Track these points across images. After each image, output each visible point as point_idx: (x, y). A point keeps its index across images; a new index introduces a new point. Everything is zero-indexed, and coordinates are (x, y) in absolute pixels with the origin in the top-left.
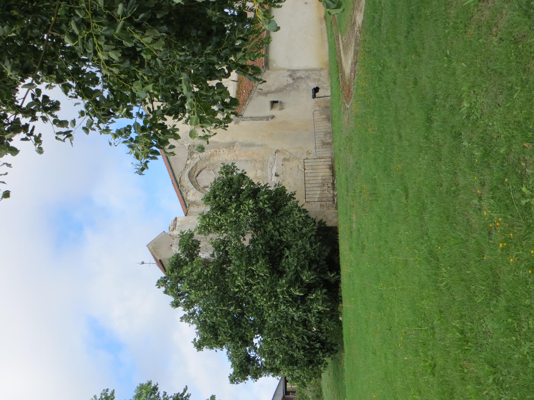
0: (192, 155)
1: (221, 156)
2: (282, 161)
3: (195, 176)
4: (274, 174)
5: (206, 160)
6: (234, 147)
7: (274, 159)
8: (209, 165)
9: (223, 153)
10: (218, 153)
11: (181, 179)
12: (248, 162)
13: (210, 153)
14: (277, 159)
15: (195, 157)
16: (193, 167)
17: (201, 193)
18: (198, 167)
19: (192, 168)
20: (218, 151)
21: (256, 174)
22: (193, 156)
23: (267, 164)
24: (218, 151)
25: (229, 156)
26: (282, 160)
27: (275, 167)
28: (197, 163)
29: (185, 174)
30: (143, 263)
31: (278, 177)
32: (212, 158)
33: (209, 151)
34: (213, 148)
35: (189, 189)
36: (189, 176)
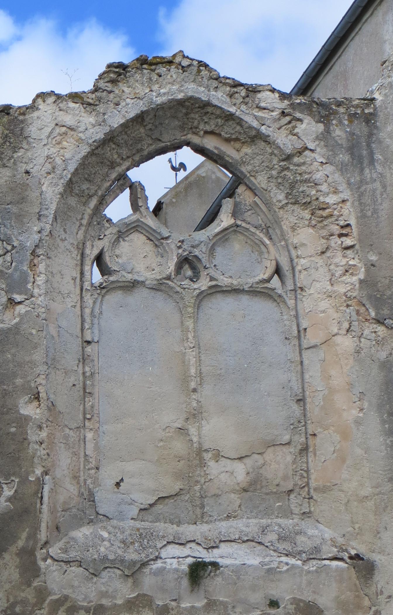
0: (311, 113)
1: (320, 261)
2: (295, 601)
3: (196, 140)
4: (208, 557)
5: (292, 186)
6: (379, 322)
7: (317, 549)
8: (268, 204)
9: (339, 271)
10: (335, 241)
11: (162, 70)
12: (296, 409)
13: (331, 199)
14: (313, 565)
15: (301, 128)
16: (240, 122)
17: (72, 167)
18: (247, 150)
19: (230, 117)
20: (348, 242)
21: (218, 456)
22: (307, 119)
23: (288, 513)
24: (348, 242)
25: (324, 304)
26: (308, 596)
27: (254, 561)
28: (266, 139)
29: (192, 86)
30: (62, 70)
31: (185, 582)
32: (306, 214)
33: (346, 194)
34: (362, 217)
35: (101, 108)
36: (181, 103)
